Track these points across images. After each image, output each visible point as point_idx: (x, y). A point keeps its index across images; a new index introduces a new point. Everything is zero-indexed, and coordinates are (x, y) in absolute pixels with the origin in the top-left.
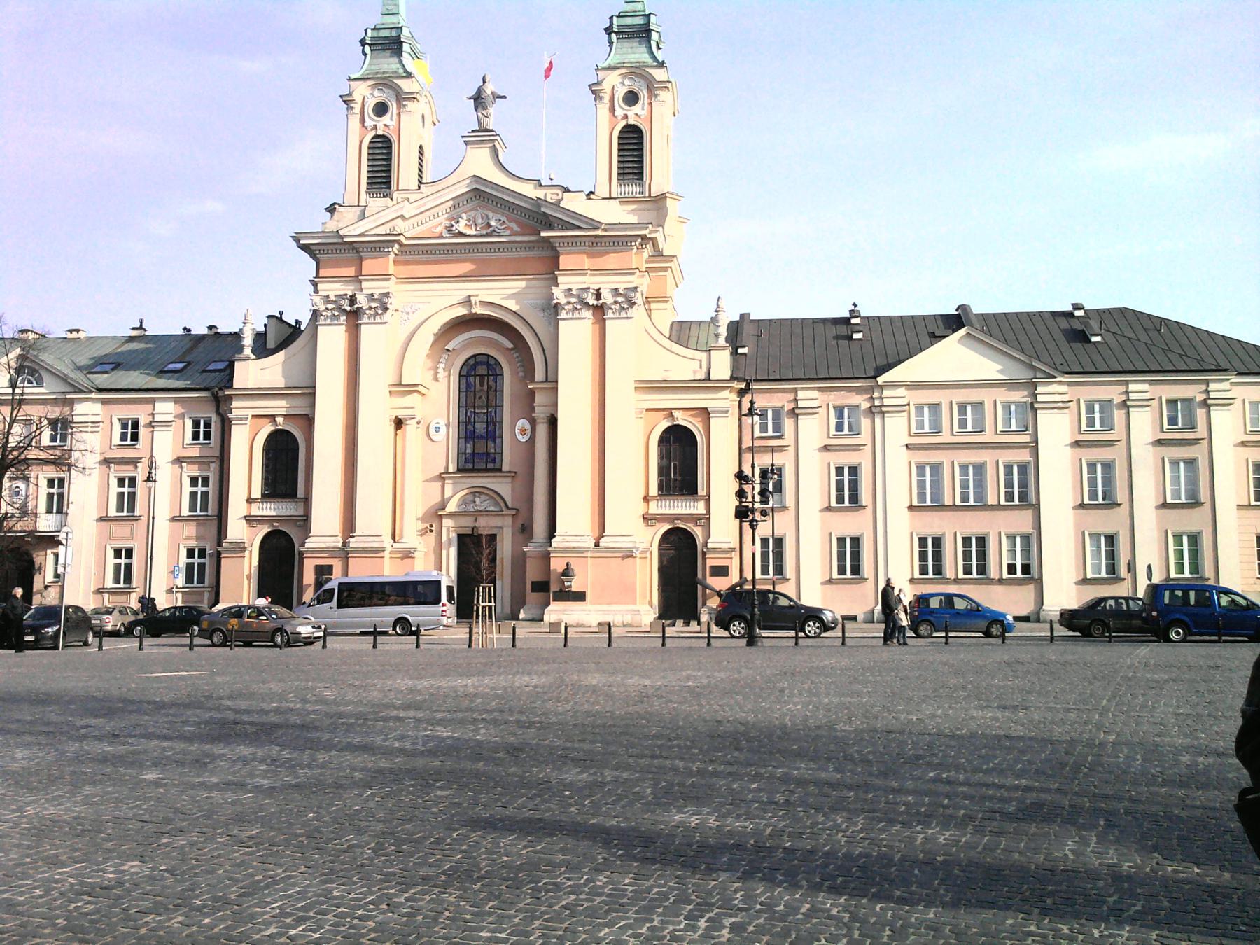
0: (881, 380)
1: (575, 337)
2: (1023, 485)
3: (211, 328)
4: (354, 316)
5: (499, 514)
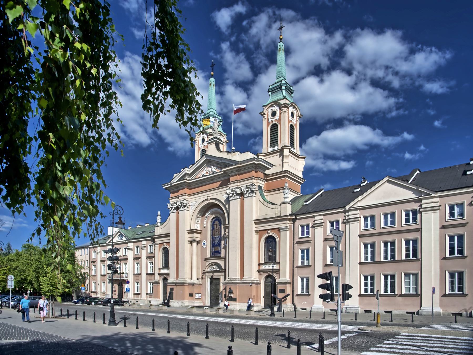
0: (347, 208)
1: (235, 205)
2: (415, 249)
4: (177, 208)
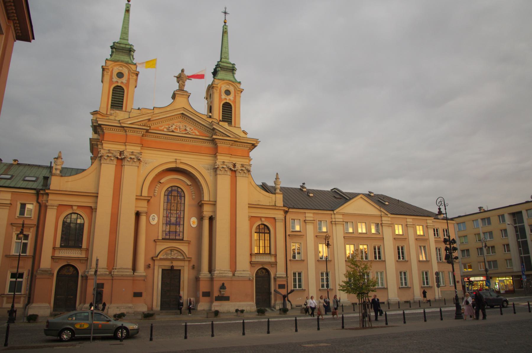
3: (15, 160)
5: (183, 260)
